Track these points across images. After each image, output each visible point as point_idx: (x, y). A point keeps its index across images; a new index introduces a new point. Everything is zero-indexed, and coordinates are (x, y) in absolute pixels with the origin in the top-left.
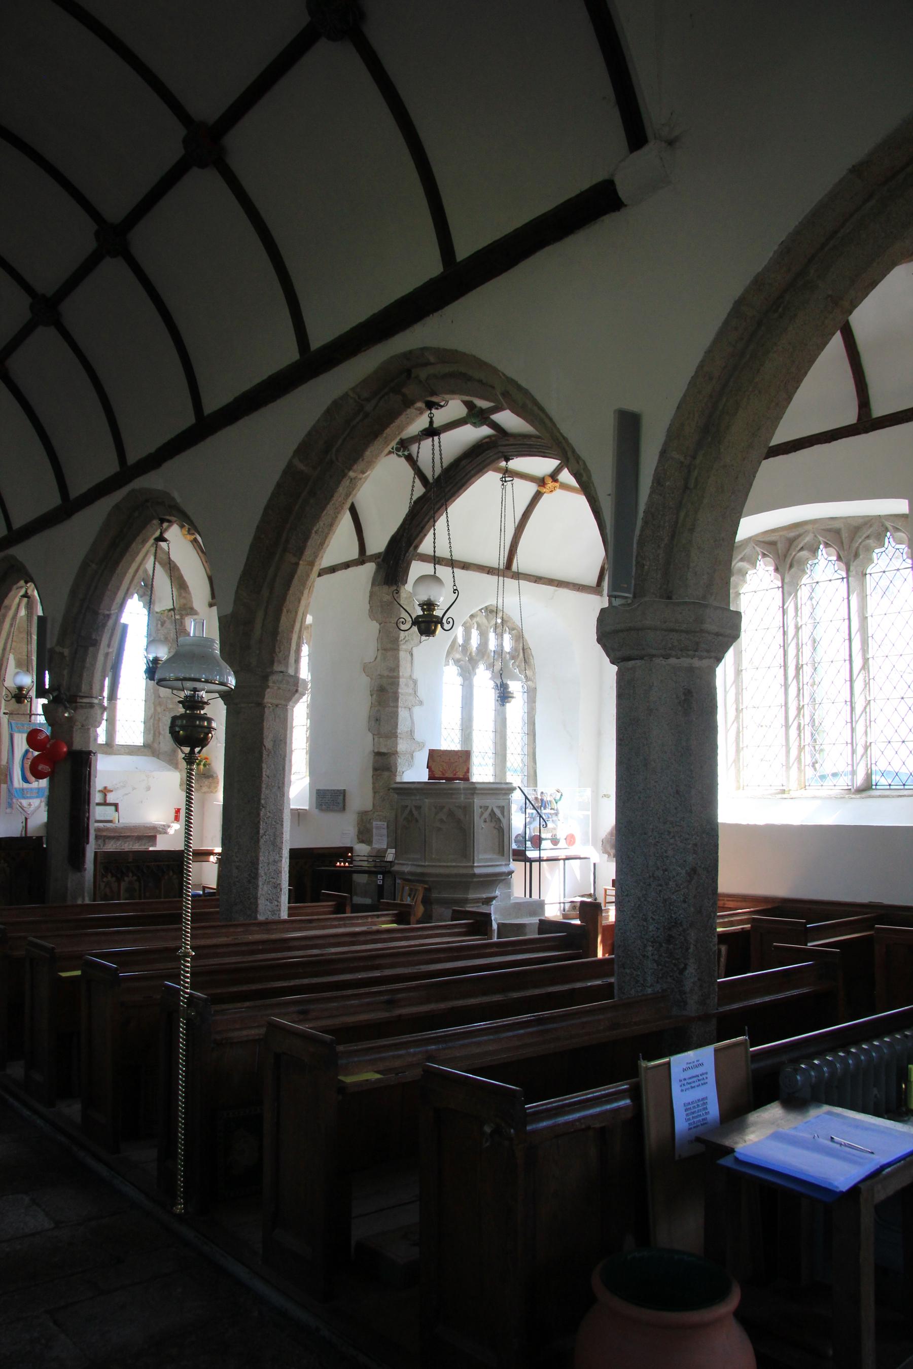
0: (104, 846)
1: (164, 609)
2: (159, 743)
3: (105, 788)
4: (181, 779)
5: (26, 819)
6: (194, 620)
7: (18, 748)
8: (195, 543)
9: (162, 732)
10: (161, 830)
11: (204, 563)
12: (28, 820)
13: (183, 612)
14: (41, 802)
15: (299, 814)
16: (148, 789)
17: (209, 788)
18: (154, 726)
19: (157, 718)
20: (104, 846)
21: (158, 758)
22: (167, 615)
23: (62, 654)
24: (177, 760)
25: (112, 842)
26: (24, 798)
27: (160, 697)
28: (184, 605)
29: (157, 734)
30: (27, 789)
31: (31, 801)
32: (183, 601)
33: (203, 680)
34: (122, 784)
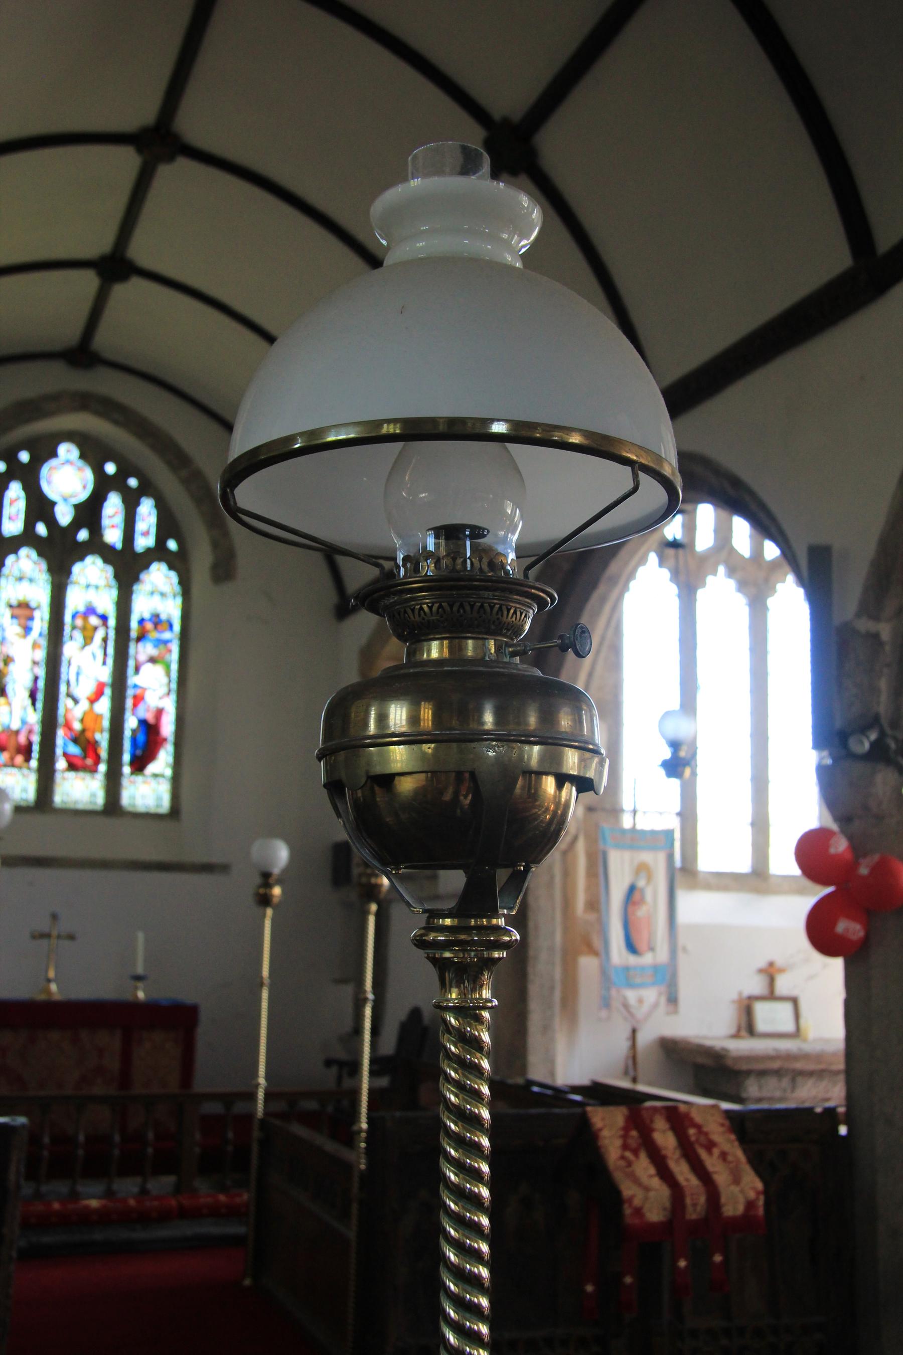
3: (771, 964)
6: (495, 640)
23: (875, 637)
25: (810, 1082)
26: (631, 986)
33: (499, 428)
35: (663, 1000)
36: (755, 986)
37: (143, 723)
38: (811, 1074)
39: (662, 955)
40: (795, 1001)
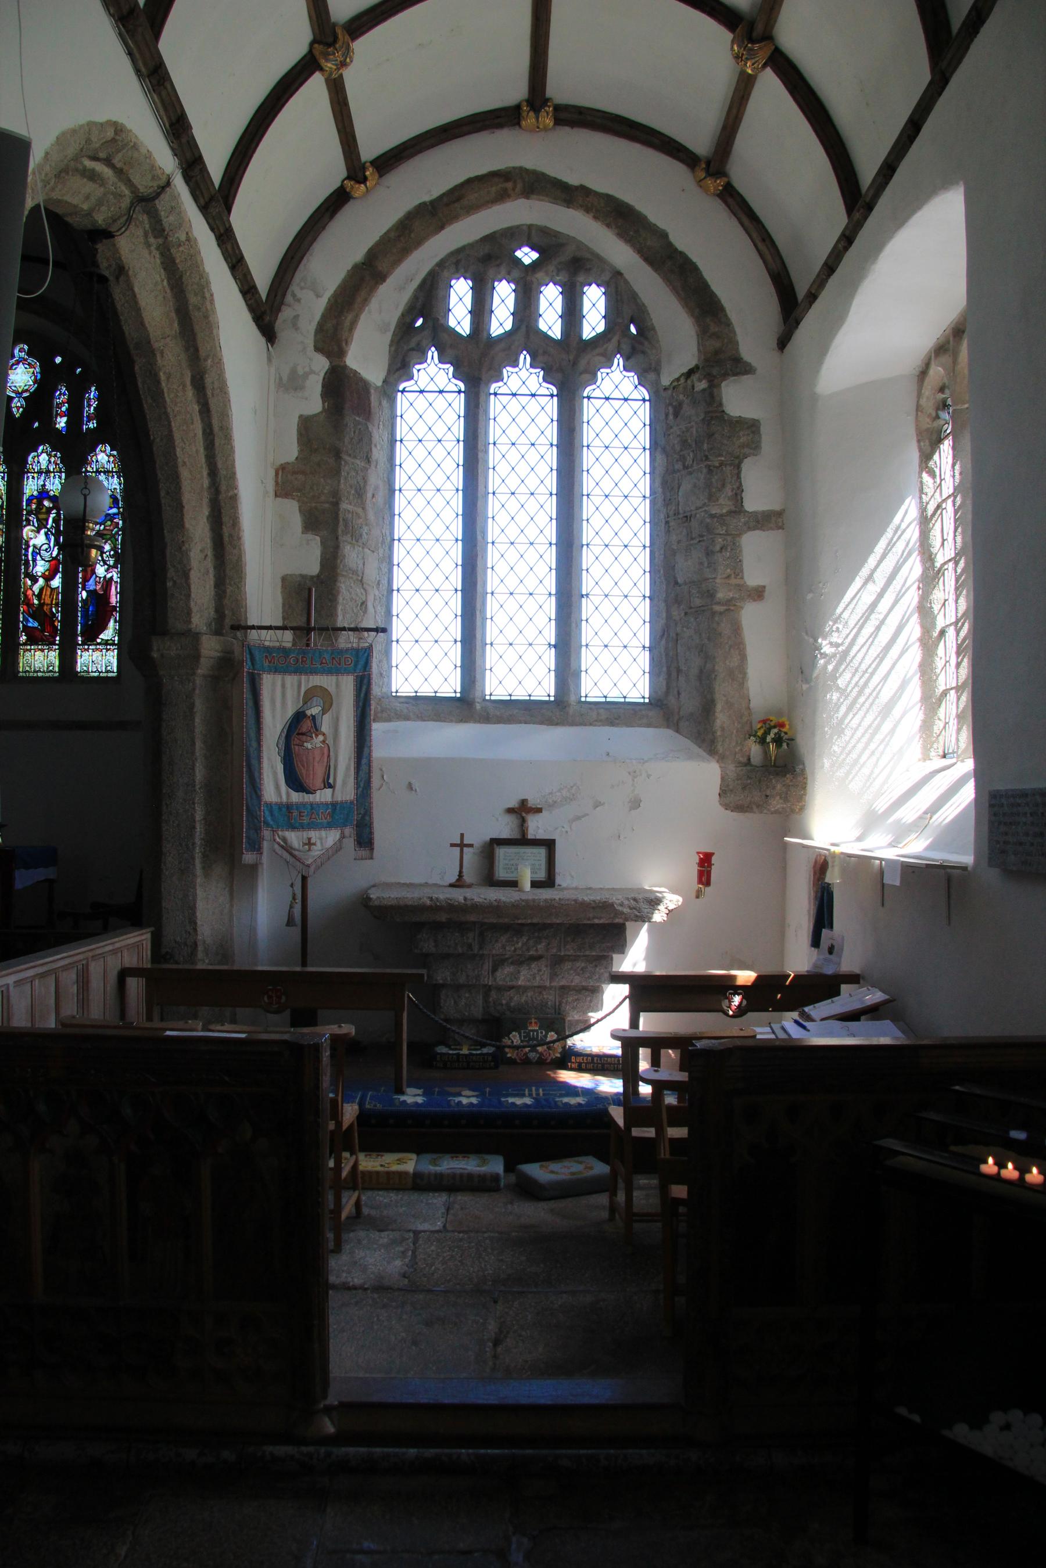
0: (481, 948)
1: (677, 376)
2: (679, 694)
3: (523, 802)
4: (723, 779)
5: (304, 879)
7: (273, 710)
8: (730, 200)
9: (684, 668)
10: (626, 910)
11: (760, 244)
12: (309, 880)
13: (715, 371)
14: (343, 836)
15: (949, 879)
16: (635, 804)
17: (786, 799)
18: (667, 655)
19: (672, 634)
20: (481, 948)
21: (677, 731)
22: (685, 388)
24: (713, 733)
26: (293, 828)
27: (676, 583)
28: (717, 352)
29: (674, 674)
30: (304, 805)
31: (314, 835)
32: (714, 344)
34: (564, 793)
35: (350, 843)
36: (505, 829)
37: (91, 593)
38: (505, 928)
39: (345, 790)
40: (549, 845)
